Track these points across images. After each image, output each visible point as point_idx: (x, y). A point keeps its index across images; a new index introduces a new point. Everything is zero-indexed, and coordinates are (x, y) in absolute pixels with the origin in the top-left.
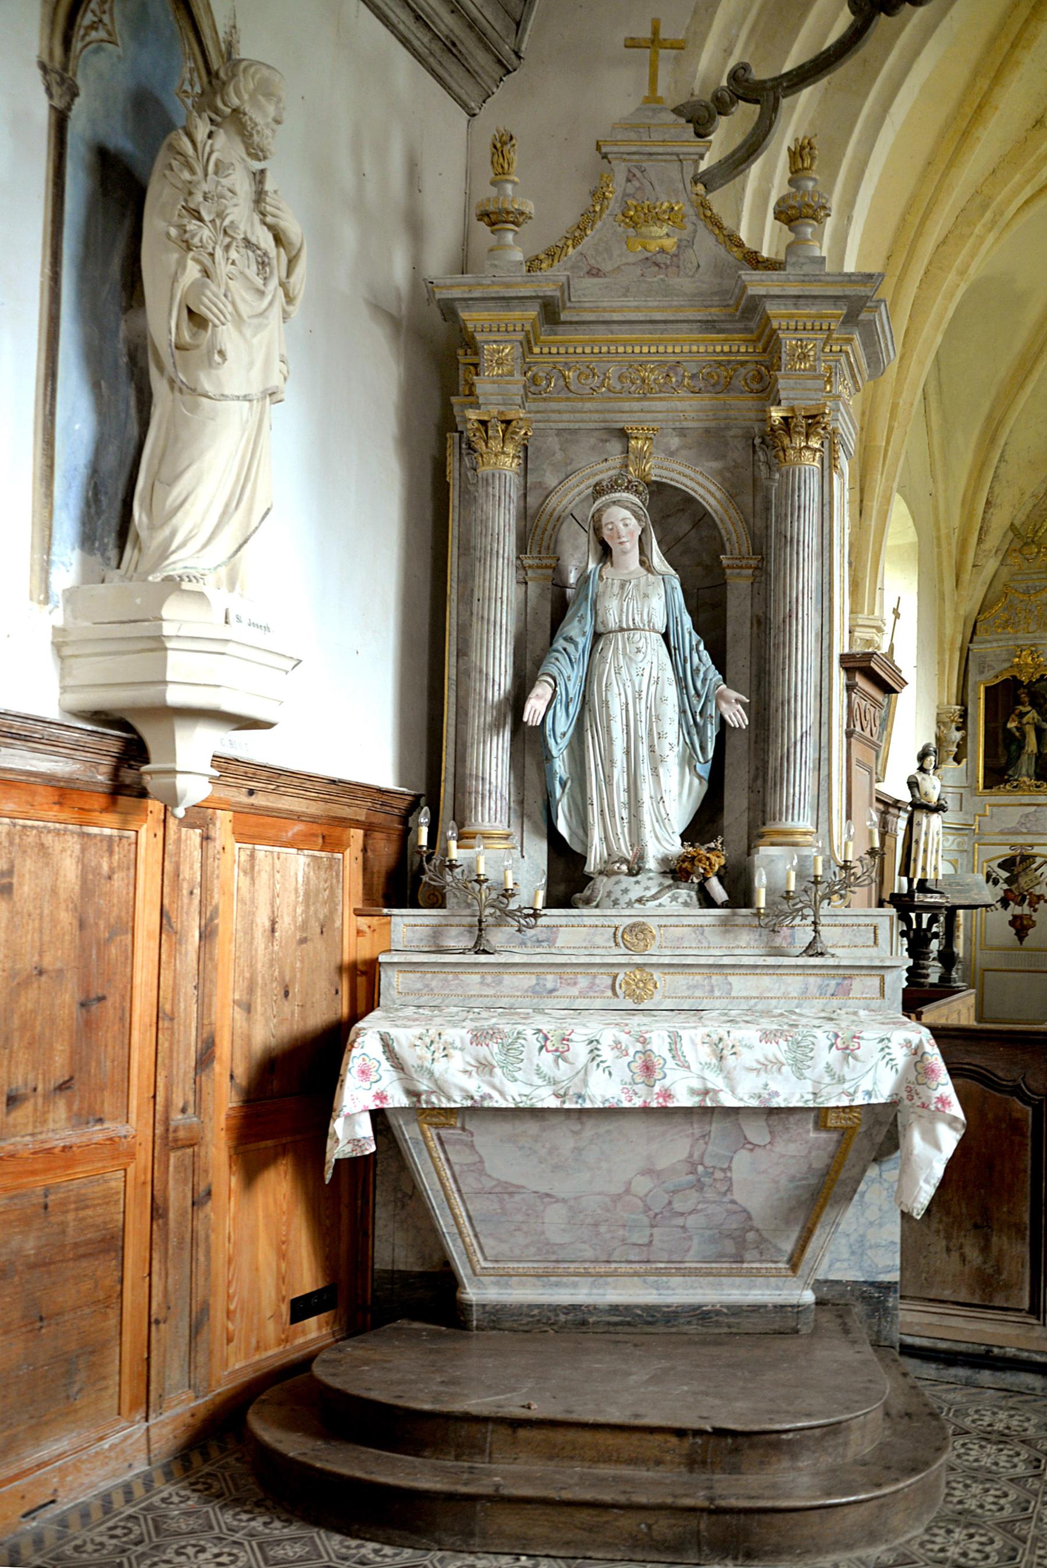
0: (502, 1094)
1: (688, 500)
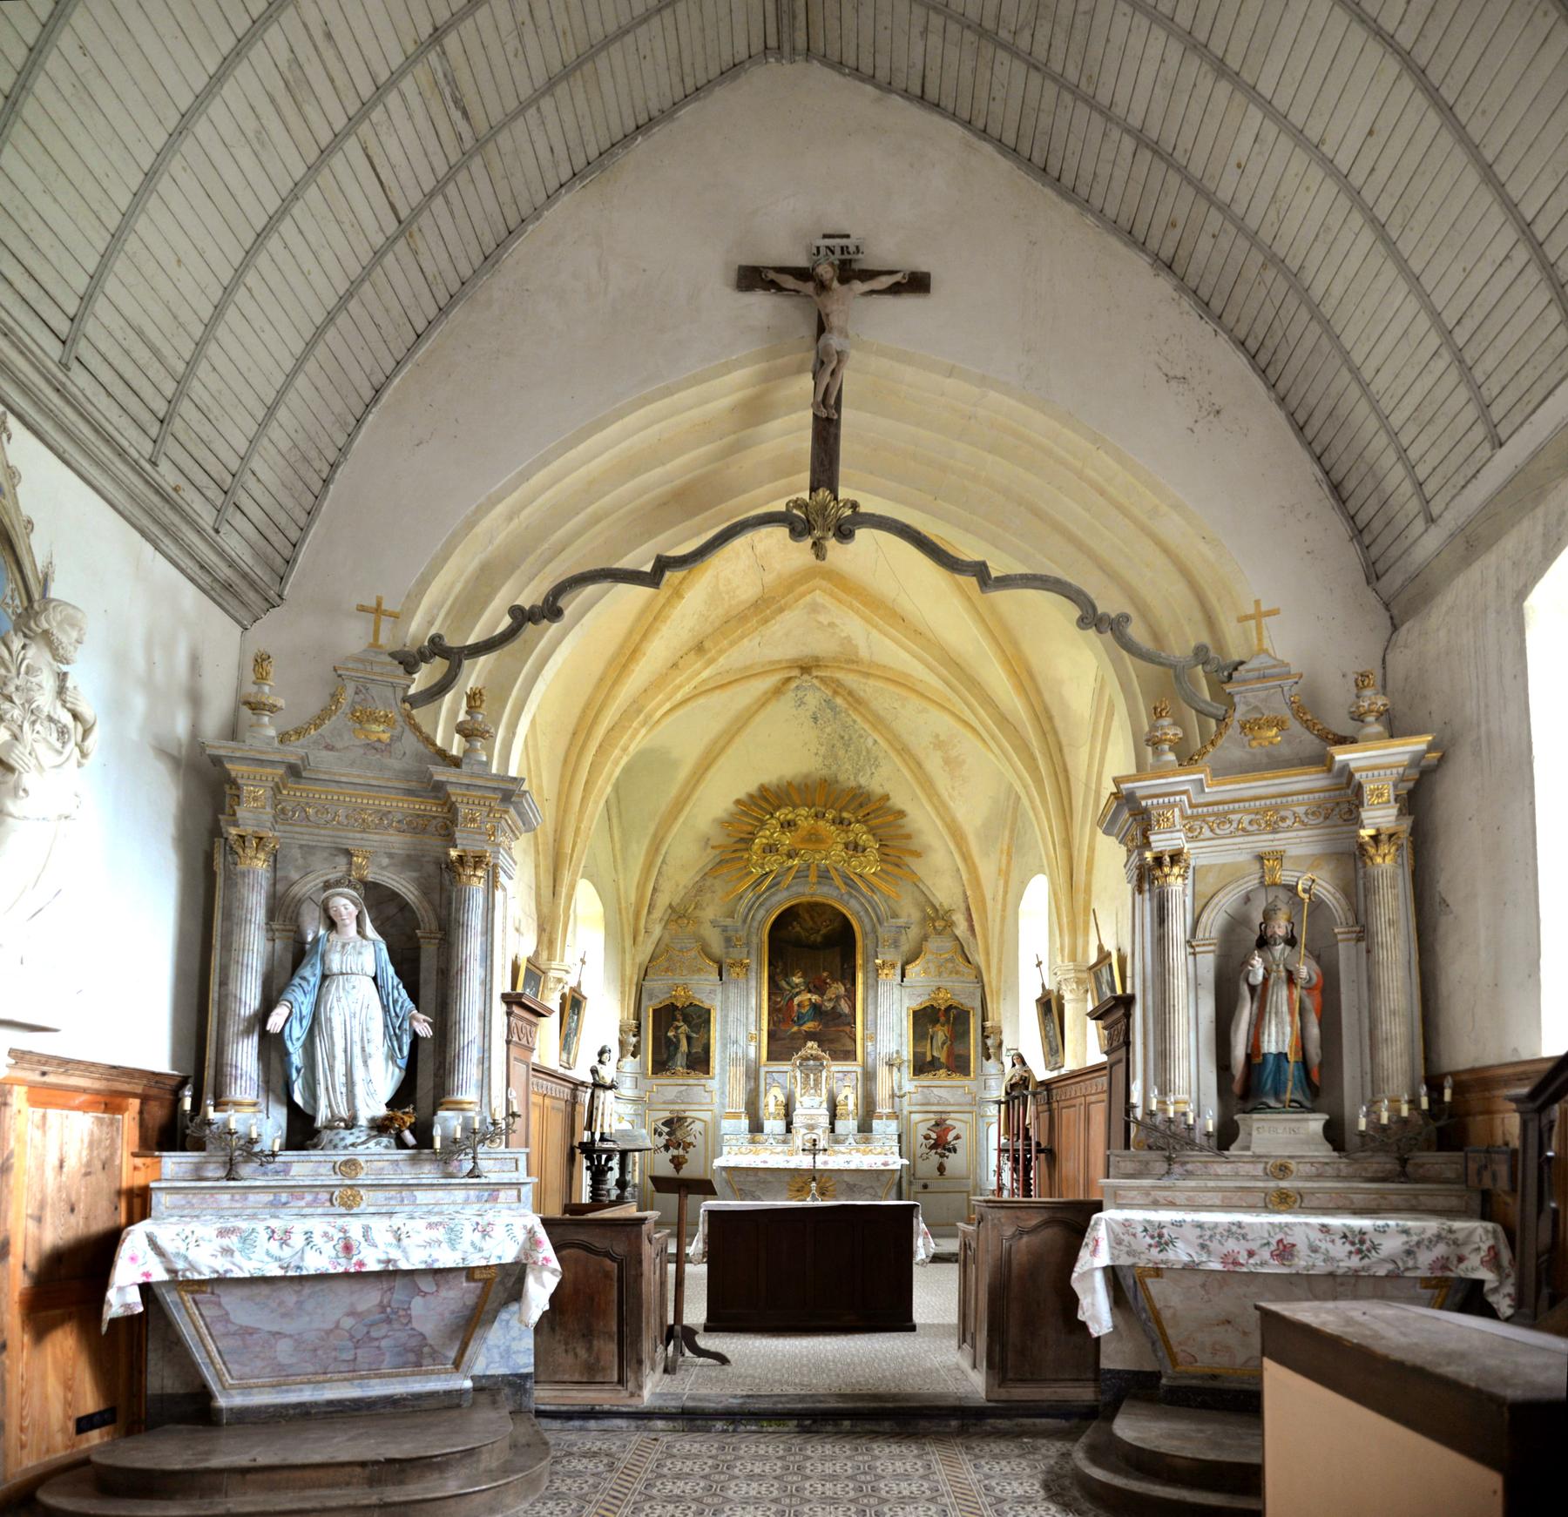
0: (240, 1268)
1: (394, 896)
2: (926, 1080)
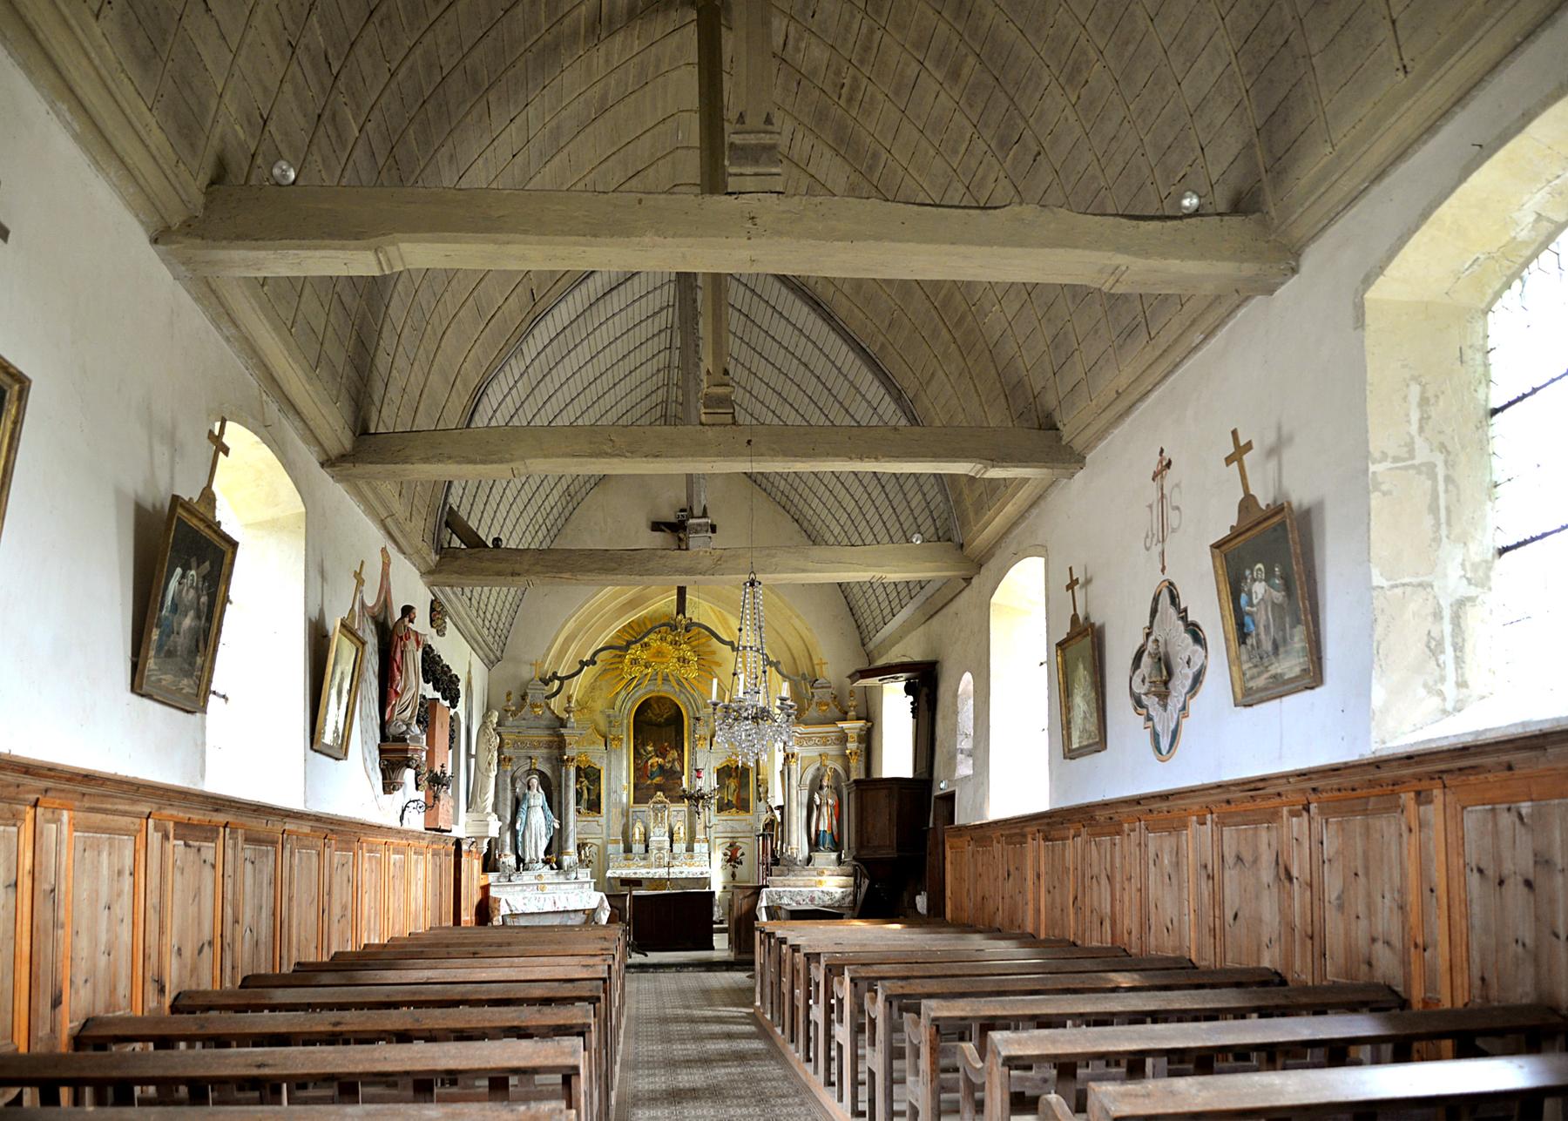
2: (724, 816)
